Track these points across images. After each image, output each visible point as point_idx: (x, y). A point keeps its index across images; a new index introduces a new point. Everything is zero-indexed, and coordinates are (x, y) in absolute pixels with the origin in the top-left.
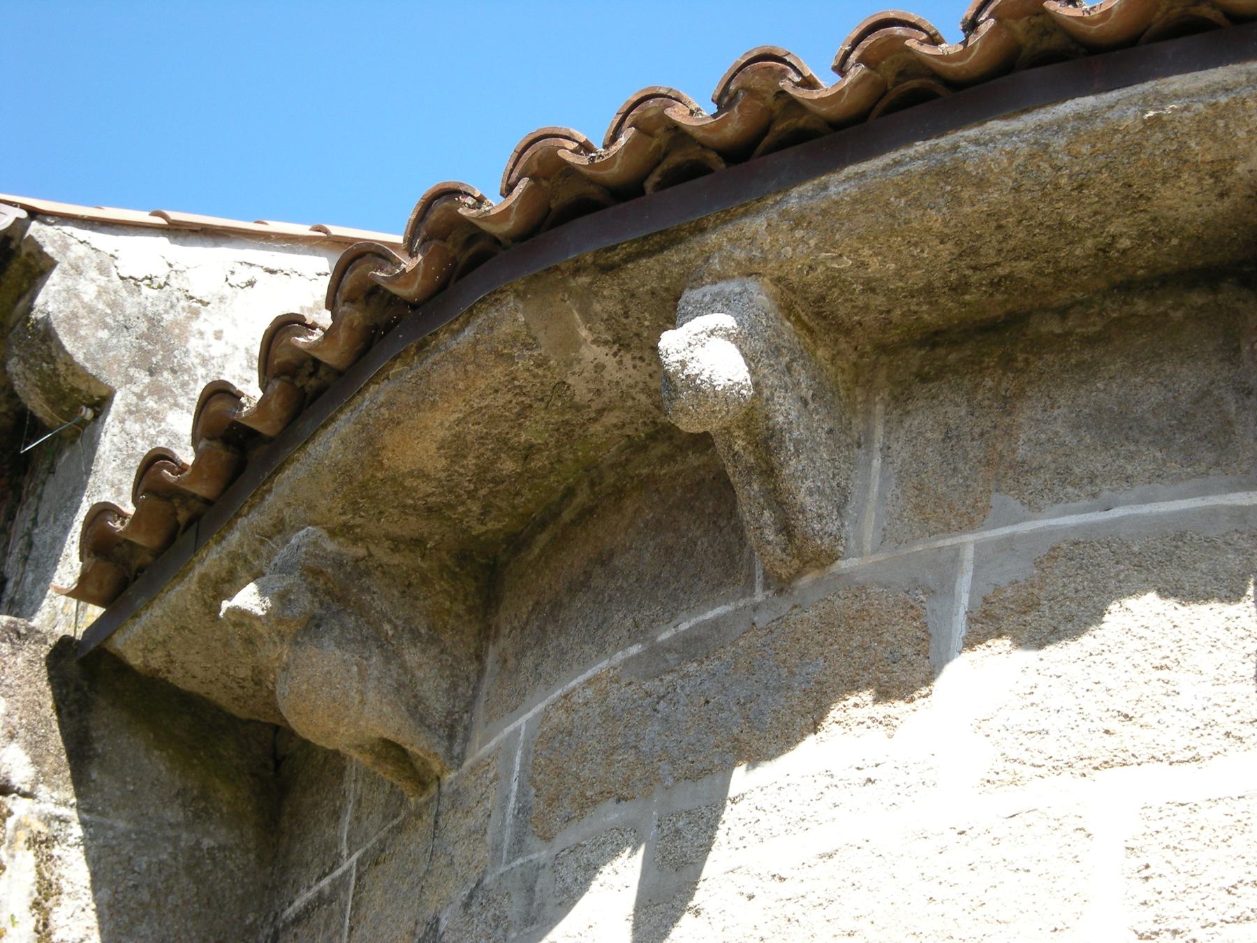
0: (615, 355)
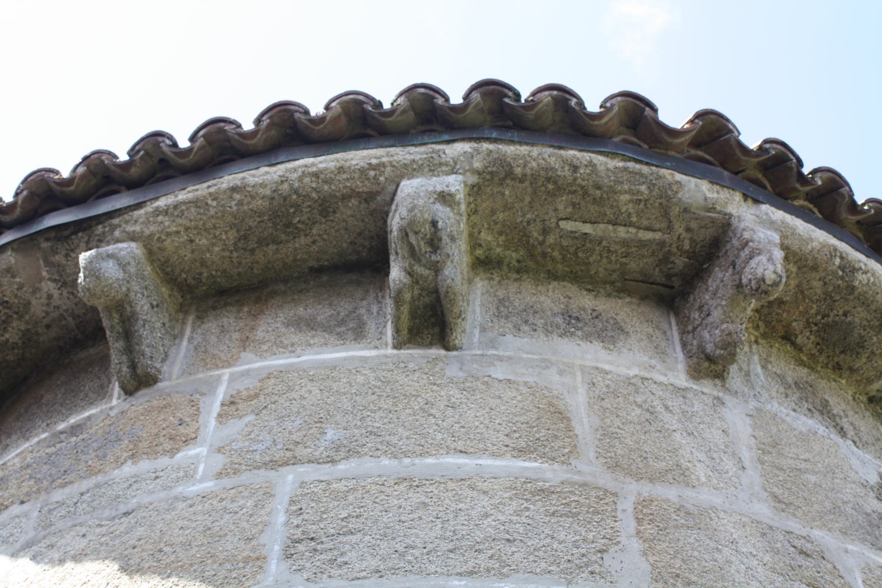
0: (59, 289)
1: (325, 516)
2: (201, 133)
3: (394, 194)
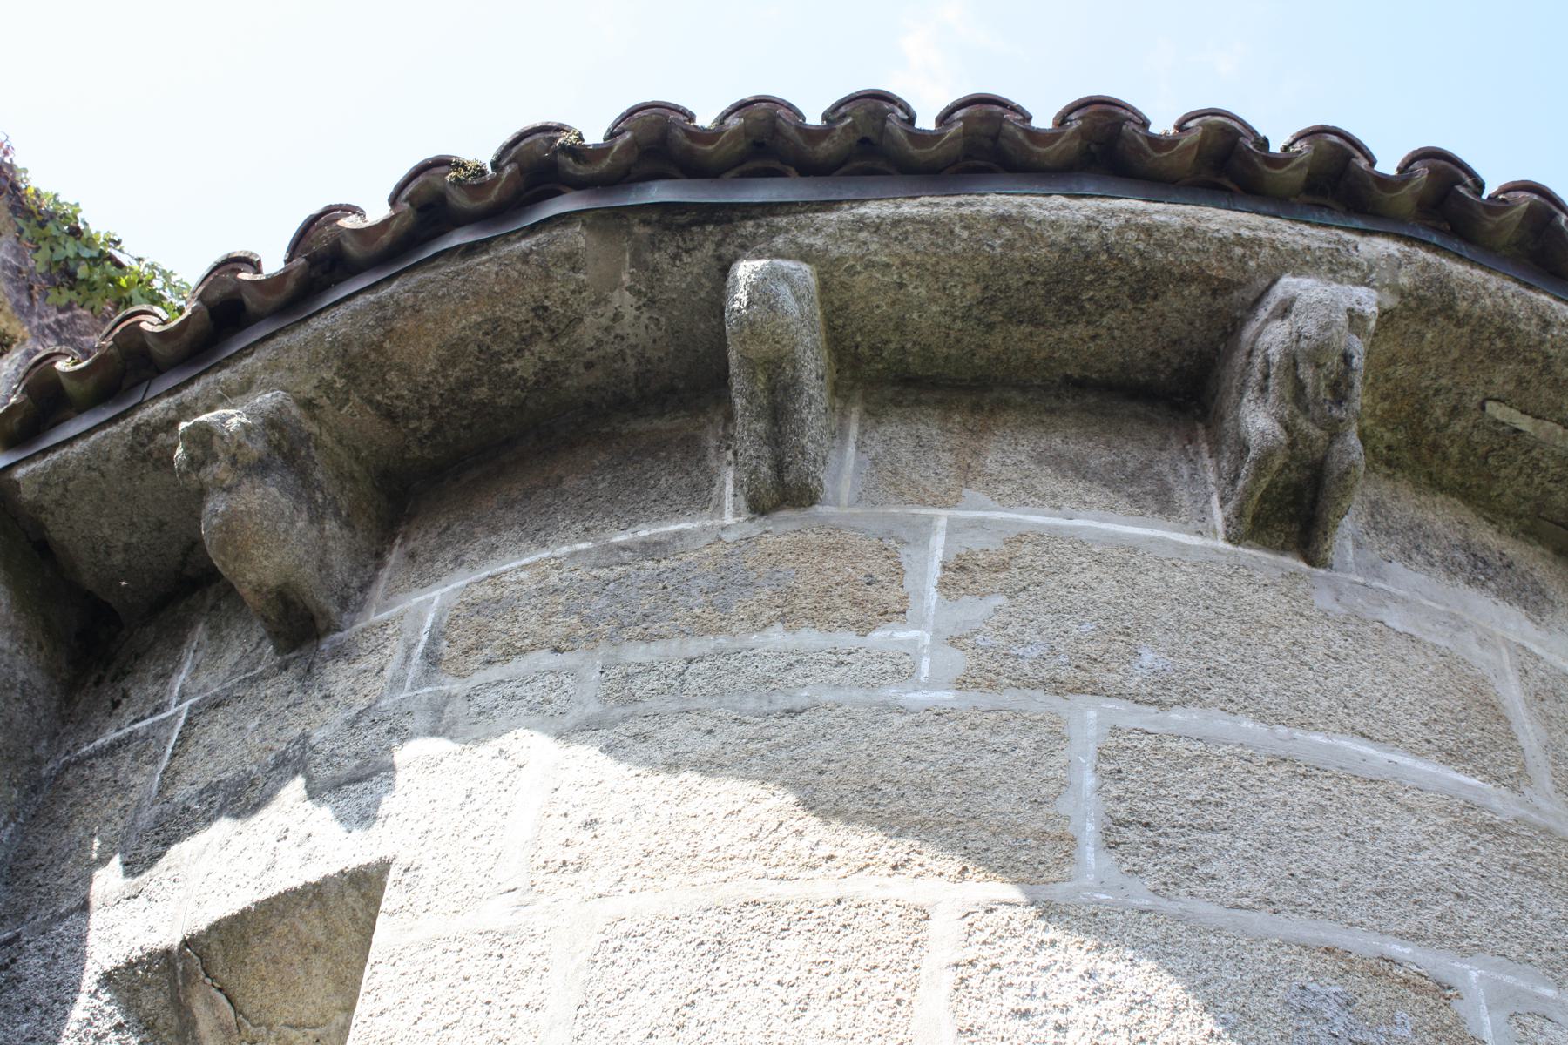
0: (638, 308)
1: (1162, 792)
2: (959, 114)
3: (1268, 289)
